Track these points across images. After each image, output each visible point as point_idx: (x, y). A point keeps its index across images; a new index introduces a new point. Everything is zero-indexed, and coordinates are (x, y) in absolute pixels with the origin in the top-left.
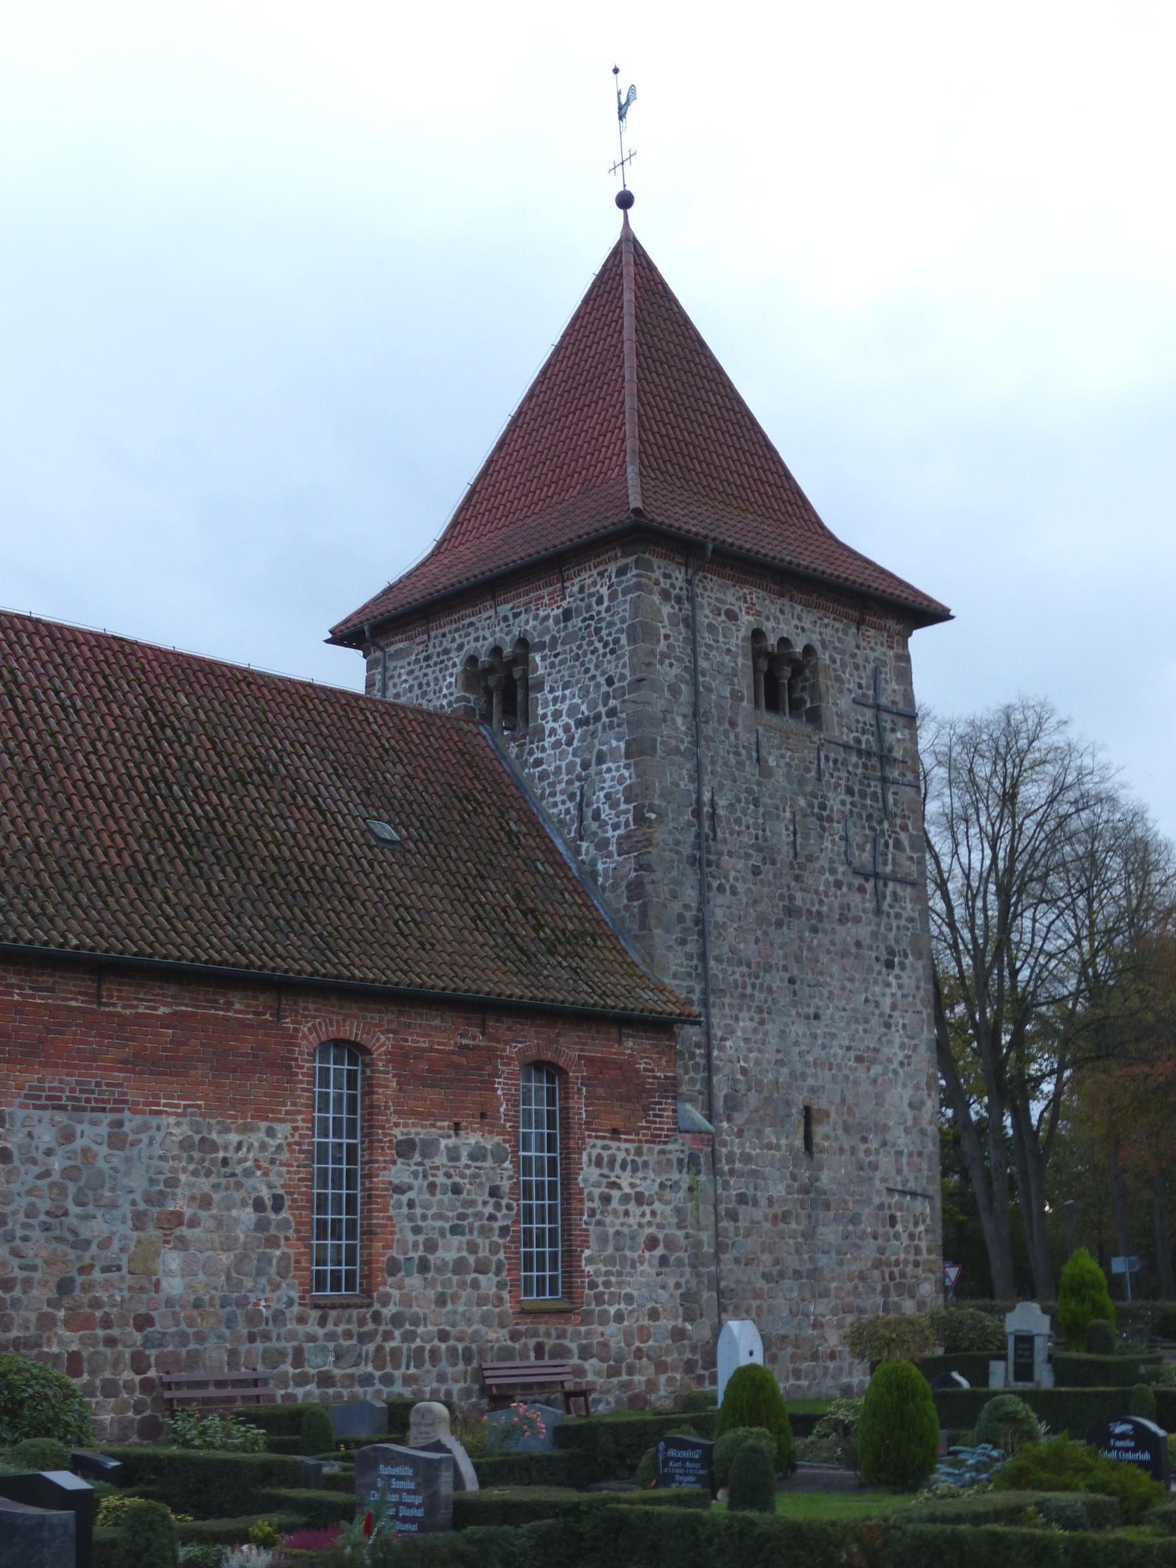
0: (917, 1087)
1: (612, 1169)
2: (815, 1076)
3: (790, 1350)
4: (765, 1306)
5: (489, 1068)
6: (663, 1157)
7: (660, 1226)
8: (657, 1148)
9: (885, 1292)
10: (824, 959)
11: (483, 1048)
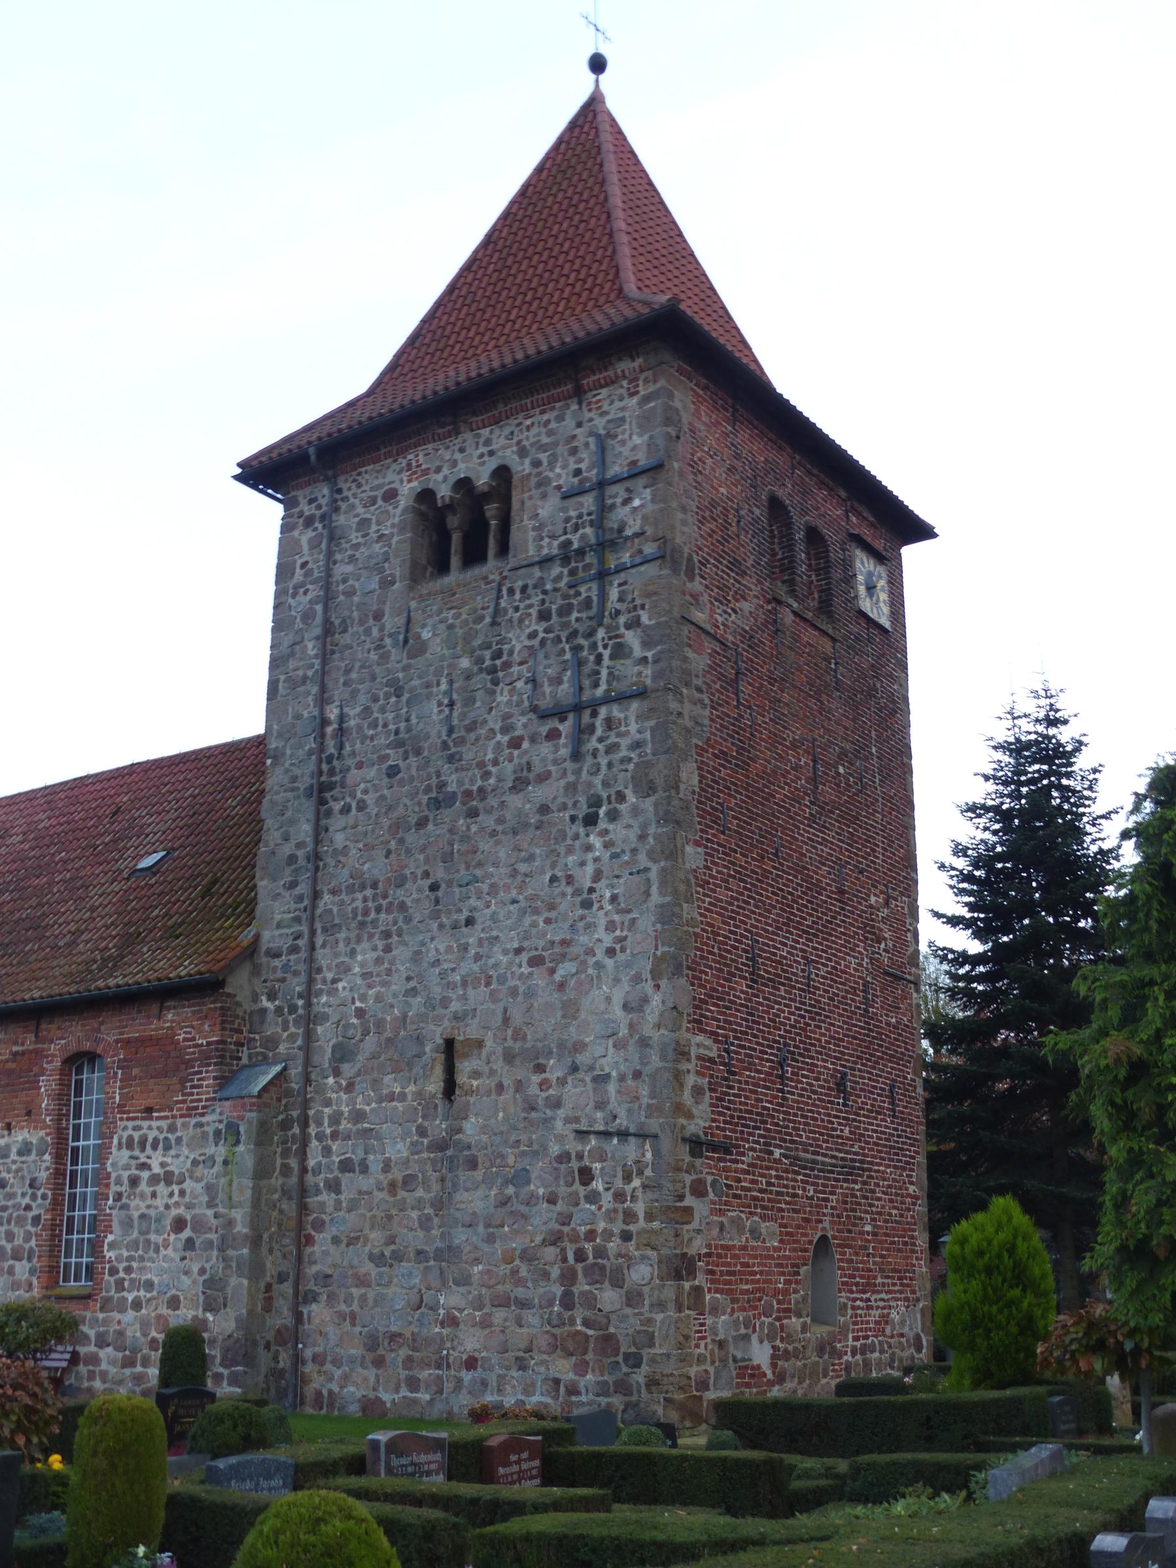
0: (637, 979)
1: (143, 1149)
2: (464, 998)
3: (403, 1352)
4: (371, 1295)
5: (36, 1069)
6: (199, 1130)
7: (189, 1206)
8: (193, 1121)
9: (569, 1277)
10: (485, 845)
11: (31, 1052)
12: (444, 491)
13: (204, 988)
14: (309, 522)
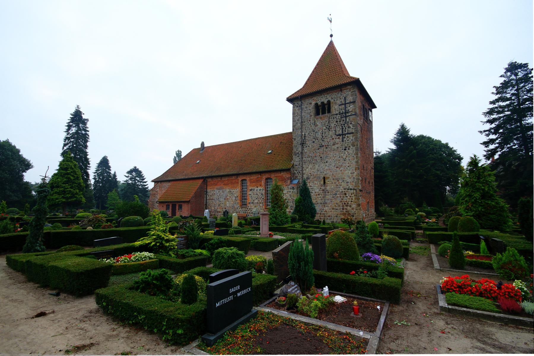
9: (343, 206)
12: (319, 104)
13: (288, 170)
14: (297, 107)
